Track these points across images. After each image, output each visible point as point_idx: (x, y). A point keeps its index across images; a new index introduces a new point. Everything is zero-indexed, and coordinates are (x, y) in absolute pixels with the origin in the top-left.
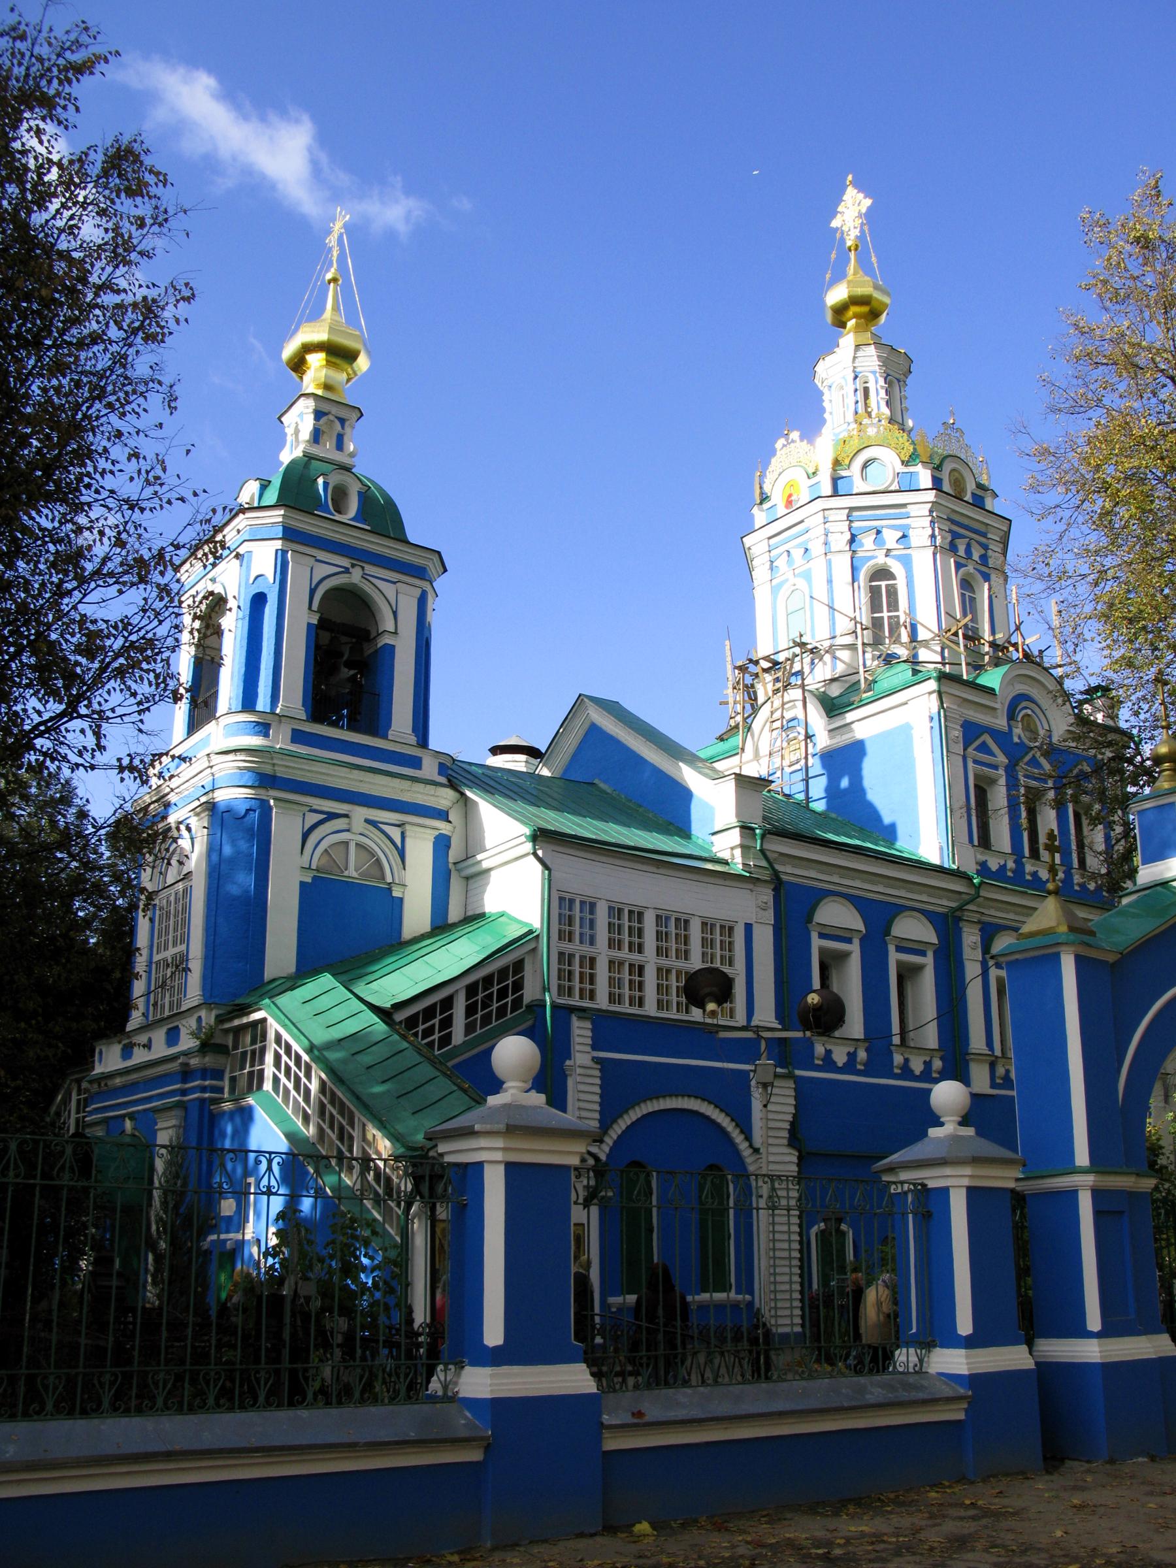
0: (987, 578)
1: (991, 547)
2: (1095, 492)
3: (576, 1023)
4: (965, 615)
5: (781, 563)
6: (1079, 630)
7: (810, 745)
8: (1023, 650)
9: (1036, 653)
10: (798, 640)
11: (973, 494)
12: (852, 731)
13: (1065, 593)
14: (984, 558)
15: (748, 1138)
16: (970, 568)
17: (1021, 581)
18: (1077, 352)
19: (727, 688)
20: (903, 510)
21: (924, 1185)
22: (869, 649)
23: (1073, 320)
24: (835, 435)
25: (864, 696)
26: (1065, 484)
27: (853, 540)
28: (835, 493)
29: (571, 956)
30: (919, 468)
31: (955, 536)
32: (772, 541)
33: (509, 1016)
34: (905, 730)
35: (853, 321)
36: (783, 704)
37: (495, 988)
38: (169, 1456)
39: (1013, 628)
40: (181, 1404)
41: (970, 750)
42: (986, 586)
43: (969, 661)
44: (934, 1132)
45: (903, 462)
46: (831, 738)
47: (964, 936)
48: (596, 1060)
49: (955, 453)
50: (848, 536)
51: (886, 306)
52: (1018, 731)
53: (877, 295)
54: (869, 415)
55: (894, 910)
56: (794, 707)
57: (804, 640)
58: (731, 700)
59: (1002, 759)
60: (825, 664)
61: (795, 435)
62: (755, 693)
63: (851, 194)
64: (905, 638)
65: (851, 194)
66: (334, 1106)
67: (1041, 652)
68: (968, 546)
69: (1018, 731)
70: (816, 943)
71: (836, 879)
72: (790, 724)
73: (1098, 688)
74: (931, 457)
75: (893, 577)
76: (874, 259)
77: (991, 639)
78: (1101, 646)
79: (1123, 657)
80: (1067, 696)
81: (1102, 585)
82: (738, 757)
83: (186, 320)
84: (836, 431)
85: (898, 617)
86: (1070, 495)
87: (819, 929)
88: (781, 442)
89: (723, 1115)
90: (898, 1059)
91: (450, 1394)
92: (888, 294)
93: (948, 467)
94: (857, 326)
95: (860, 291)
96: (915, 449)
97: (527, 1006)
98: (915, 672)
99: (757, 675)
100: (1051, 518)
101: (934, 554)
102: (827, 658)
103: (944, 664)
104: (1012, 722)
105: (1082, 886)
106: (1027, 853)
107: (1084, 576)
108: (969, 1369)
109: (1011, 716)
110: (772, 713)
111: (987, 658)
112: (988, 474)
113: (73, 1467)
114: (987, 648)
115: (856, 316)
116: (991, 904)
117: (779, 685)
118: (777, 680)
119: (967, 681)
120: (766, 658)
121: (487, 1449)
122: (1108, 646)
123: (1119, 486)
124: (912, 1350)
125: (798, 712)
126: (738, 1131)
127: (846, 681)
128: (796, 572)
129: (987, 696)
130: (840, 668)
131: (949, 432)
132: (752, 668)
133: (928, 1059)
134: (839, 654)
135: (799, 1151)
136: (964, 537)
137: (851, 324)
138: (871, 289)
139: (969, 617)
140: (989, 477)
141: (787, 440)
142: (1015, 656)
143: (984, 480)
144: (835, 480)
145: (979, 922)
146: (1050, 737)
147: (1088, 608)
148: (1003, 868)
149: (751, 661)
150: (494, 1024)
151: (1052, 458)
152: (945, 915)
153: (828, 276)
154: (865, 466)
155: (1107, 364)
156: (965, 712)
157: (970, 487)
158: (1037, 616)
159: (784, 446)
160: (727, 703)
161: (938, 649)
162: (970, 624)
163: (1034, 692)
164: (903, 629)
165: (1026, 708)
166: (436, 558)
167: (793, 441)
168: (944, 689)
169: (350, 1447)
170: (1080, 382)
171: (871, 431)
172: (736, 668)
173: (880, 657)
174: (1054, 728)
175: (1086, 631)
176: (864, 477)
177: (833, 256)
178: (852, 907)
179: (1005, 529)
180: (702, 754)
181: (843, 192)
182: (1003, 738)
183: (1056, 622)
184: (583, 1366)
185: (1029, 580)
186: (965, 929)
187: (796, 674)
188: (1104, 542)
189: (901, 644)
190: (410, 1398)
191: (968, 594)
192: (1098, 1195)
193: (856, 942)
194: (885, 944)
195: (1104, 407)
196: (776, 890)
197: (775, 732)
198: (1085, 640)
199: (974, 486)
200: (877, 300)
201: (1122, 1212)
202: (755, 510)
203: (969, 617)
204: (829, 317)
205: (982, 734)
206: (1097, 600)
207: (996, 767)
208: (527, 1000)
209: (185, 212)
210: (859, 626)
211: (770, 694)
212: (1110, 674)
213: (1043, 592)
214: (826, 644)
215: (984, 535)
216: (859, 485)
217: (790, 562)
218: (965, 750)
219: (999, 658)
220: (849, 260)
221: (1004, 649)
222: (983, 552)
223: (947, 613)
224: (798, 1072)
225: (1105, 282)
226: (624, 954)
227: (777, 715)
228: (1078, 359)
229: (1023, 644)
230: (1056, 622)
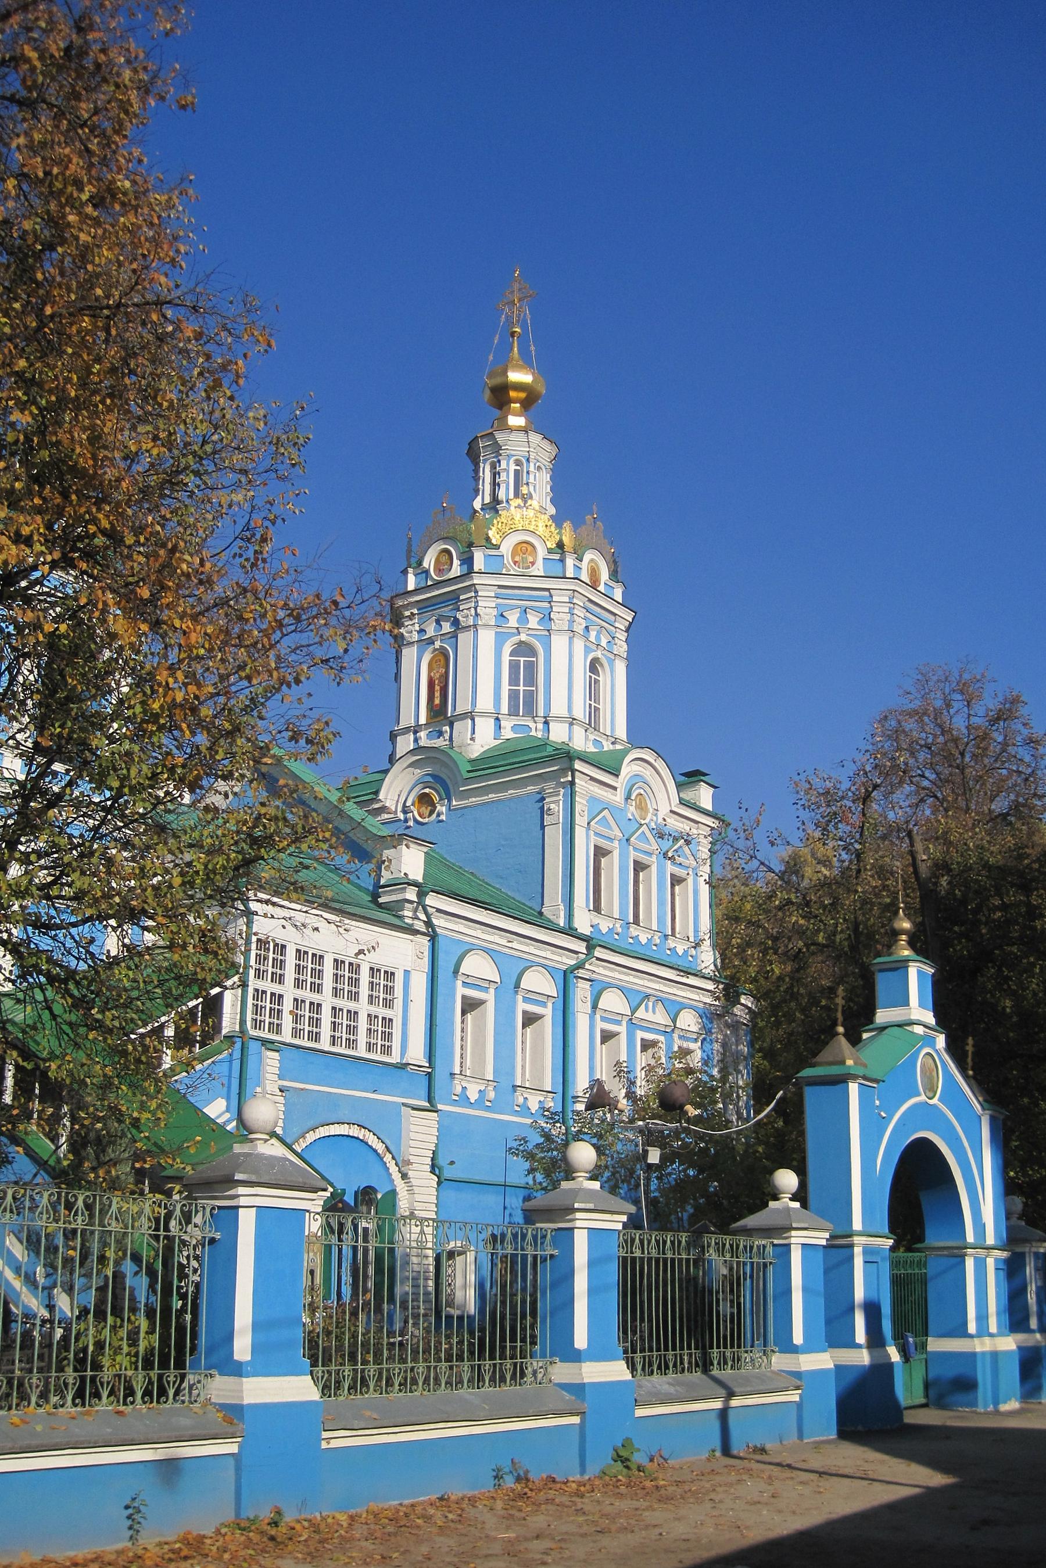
44: (772, 1204)
70: (461, 991)
76: (532, 348)
87: (464, 978)
133: (483, 1088)
135: (438, 1177)
156: (592, 788)
207: (611, 840)
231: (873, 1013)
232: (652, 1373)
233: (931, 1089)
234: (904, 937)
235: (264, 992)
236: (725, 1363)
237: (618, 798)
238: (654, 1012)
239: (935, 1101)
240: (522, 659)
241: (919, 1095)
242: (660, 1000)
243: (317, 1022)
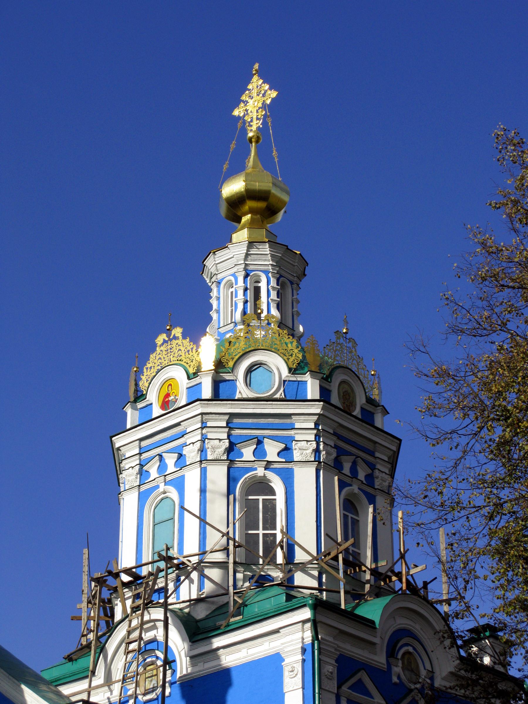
0: (372, 500)
1: (378, 466)
2: (493, 419)
4: (346, 538)
5: (153, 470)
6: (471, 565)
7: (169, 673)
8: (407, 580)
9: (420, 585)
10: (164, 553)
11: (362, 409)
12: (218, 658)
13: (458, 525)
14: (370, 478)
16: (355, 488)
17: (411, 508)
18: (482, 272)
19: (82, 602)
20: (288, 421)
22: (240, 569)
23: (480, 238)
24: (219, 334)
25: (232, 620)
26: (462, 409)
27: (230, 449)
28: (216, 397)
30: (307, 378)
31: (341, 452)
32: (144, 444)
35: (249, 216)
36: (143, 623)
39: (397, 556)
41: (344, 688)
42: (371, 510)
43: (348, 588)
45: (290, 370)
46: (193, 665)
50: (226, 444)
51: (284, 203)
52: (397, 670)
53: (275, 191)
54: (259, 316)
56: (155, 627)
57: (171, 553)
58: (84, 616)
60: (191, 581)
61: (178, 331)
62: (112, 610)
63: (256, 82)
64: (280, 559)
65: (256, 82)
67: (426, 584)
69: (397, 670)
72: (149, 647)
73: (487, 627)
74: (320, 366)
75: (272, 492)
76: (275, 153)
77: (373, 566)
78: (492, 585)
79: (517, 599)
80: (452, 634)
81: (497, 519)
82: (87, 681)
84: (222, 330)
85: (275, 535)
86: (467, 421)
88: (163, 337)
92: (287, 193)
93: (338, 378)
94: (252, 220)
95: (257, 186)
96: (304, 357)
98: (289, 598)
99: (115, 590)
100: (446, 444)
102: (195, 575)
103: (320, 590)
104: (391, 660)
107: (479, 508)
109: (391, 653)
110: (129, 633)
111: (367, 587)
112: (379, 389)
114: (368, 576)
115: (251, 211)
117: (140, 602)
118: (137, 596)
119: (345, 611)
120: (128, 571)
122: (502, 586)
123: (520, 416)
125: (159, 634)
127: (213, 603)
128: (169, 478)
130: (208, 587)
131: (342, 341)
132: (111, 581)
134: (207, 572)
136: (349, 454)
137: (246, 218)
138: (271, 185)
139: (351, 541)
140: (380, 392)
141: (168, 336)
142: (398, 586)
143: (375, 394)
144: (216, 384)
146: (432, 679)
147: (482, 543)
149: (110, 573)
151: (451, 381)
153: (225, 167)
154: (250, 370)
155: (514, 288)
157: (360, 400)
158: (427, 548)
159: (165, 341)
160: (80, 619)
161: (316, 573)
162: (351, 548)
163: (417, 627)
164: (279, 551)
165: (407, 645)
167: (175, 338)
168: (320, 618)
170: (490, 308)
171: (259, 334)
172: (93, 580)
173: (252, 577)
174: (437, 670)
175: (478, 568)
176: (248, 383)
177: (233, 146)
179: (394, 448)
180: (46, 675)
181: (249, 81)
183: (444, 554)
185: (420, 508)
187: (159, 590)
188: (502, 472)
189: (276, 565)
191: (350, 515)
195: (508, 331)
197: (130, 656)
198: (477, 577)
199: (364, 401)
200: (275, 196)
202: (129, 410)
203: (351, 541)
204: (223, 209)
205: (359, 671)
206: (492, 534)
210: (231, 543)
211: (129, 611)
212: (502, 617)
213: (434, 522)
214: (195, 560)
218: (339, 687)
219: (379, 587)
220: (249, 151)
221: (386, 577)
222: (370, 471)
223: (327, 535)
225: (516, 203)
227: (135, 635)
228: (484, 279)
229: (408, 573)
230: (444, 554)
240: (261, 498)
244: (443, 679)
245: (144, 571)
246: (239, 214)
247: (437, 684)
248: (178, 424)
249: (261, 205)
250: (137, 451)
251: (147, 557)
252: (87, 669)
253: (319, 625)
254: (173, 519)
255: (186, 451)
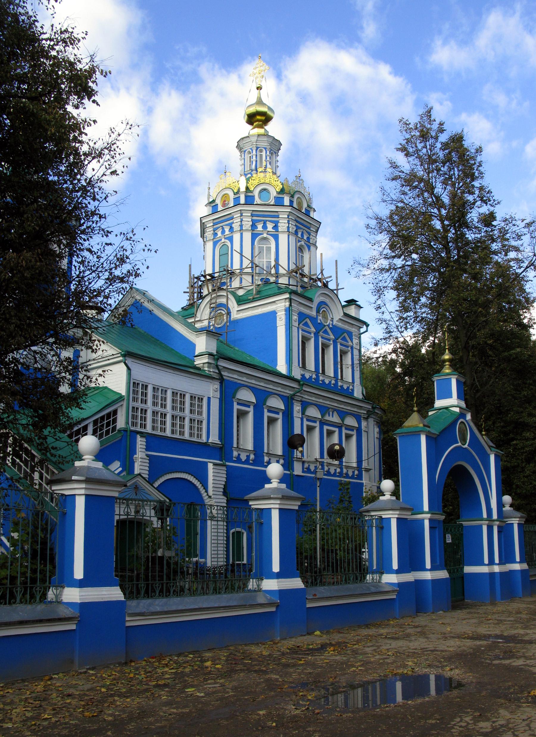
3: (139, 438)
15: (207, 491)
16: (303, 243)
21: (381, 517)
29: (137, 409)
32: (215, 221)
33: (110, 434)
34: (274, 314)
37: (105, 422)
38: (40, 621)
40: (27, 601)
41: (301, 325)
47: (295, 406)
48: (147, 455)
49: (299, 190)
52: (320, 318)
55: (268, 394)
59: (313, 329)
66: (48, 474)
68: (302, 233)
71: (244, 379)
83: (127, 167)
89: (197, 481)
90: (235, 454)
91: (59, 600)
93: (296, 196)
97: (118, 430)
101: (289, 236)
104: (318, 314)
105: (323, 381)
106: (321, 372)
108: (80, 599)
109: (318, 311)
110: (211, 300)
113: (149, 615)
116: (306, 393)
120: (209, 275)
121: (277, 607)
124: (254, 580)
126: (203, 488)
129: (309, 302)
135: (227, 497)
145: (301, 401)
146: (332, 321)
148: (311, 377)
150: (104, 438)
152: (288, 397)
157: (305, 205)
163: (327, 301)
166: (365, 330)
168: (292, 297)
169: (22, 623)
176: (260, 198)
178: (251, 392)
182: (313, 320)
184: (299, 579)
186: (295, 404)
190: (160, 596)
192: (431, 520)
193: (281, 414)
194: (263, 409)
196: (221, 383)
199: (306, 206)
201: (436, 527)
207: (329, 340)
208: (118, 428)
209: (138, 126)
215: (309, 229)
216: (257, 200)
217: (223, 232)
218: (299, 325)
224: (227, 463)
226: (158, 408)
227: (213, 301)
231: (433, 403)
232: (317, 584)
233: (464, 440)
234: (447, 363)
235: (137, 409)
236: (357, 579)
237: (314, 313)
238: (333, 416)
239: (466, 446)
240: (265, 246)
241: (458, 443)
242: (334, 410)
243: (164, 423)
244: (337, 321)
245: (216, 275)
246: (253, 121)
247: (334, 324)
248: (230, 214)
249: (263, 118)
250: (212, 224)
251: (217, 270)
252: (194, 314)
253: (292, 301)
254: (228, 254)
255: (233, 225)
